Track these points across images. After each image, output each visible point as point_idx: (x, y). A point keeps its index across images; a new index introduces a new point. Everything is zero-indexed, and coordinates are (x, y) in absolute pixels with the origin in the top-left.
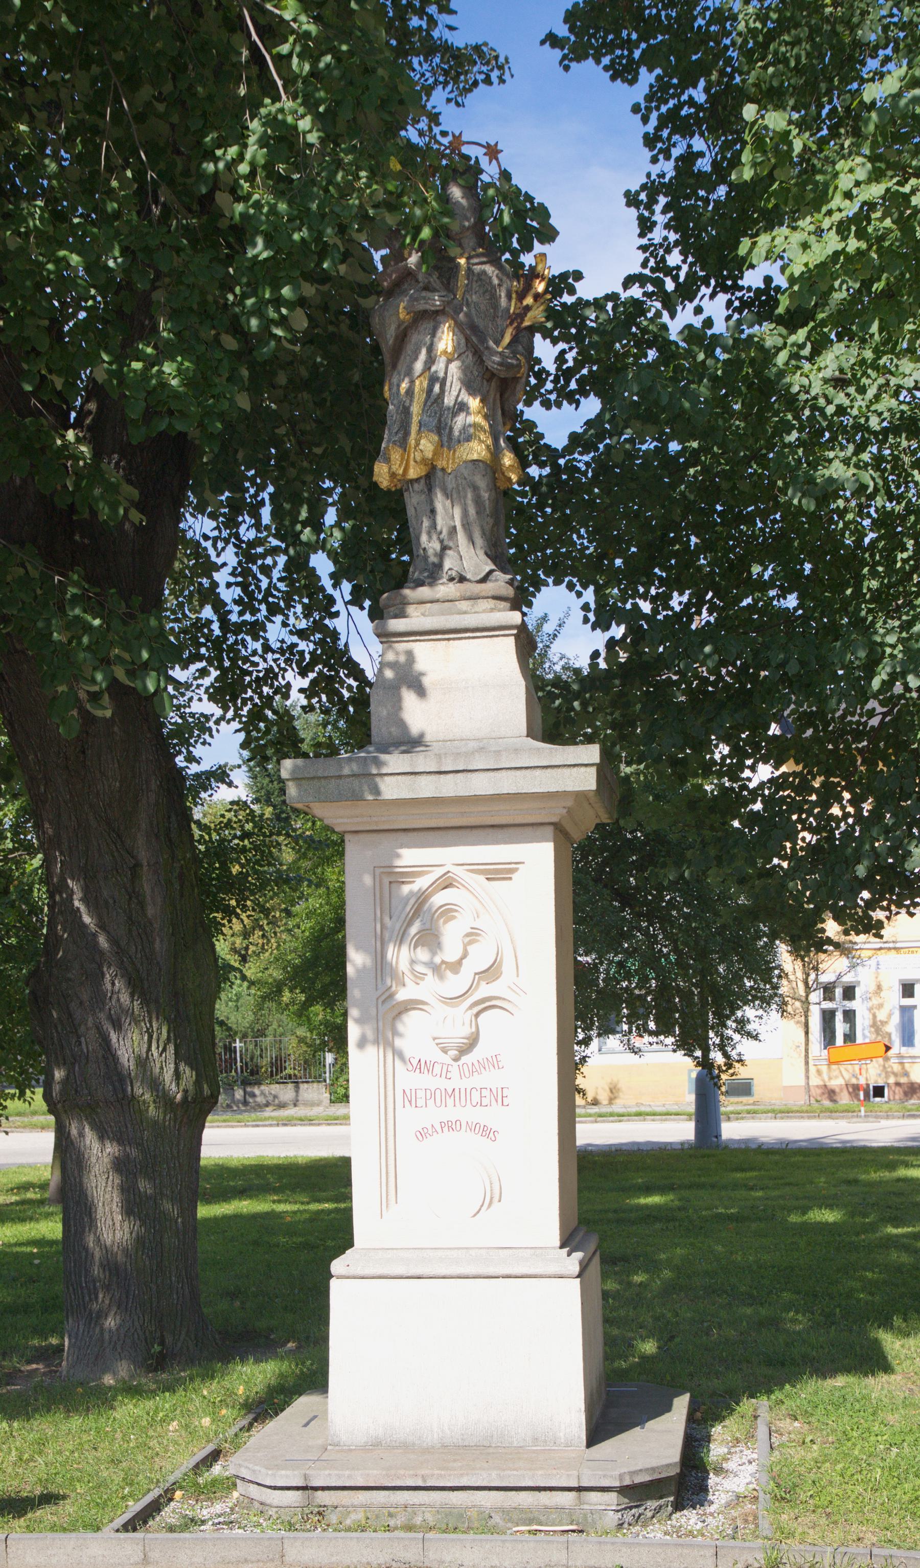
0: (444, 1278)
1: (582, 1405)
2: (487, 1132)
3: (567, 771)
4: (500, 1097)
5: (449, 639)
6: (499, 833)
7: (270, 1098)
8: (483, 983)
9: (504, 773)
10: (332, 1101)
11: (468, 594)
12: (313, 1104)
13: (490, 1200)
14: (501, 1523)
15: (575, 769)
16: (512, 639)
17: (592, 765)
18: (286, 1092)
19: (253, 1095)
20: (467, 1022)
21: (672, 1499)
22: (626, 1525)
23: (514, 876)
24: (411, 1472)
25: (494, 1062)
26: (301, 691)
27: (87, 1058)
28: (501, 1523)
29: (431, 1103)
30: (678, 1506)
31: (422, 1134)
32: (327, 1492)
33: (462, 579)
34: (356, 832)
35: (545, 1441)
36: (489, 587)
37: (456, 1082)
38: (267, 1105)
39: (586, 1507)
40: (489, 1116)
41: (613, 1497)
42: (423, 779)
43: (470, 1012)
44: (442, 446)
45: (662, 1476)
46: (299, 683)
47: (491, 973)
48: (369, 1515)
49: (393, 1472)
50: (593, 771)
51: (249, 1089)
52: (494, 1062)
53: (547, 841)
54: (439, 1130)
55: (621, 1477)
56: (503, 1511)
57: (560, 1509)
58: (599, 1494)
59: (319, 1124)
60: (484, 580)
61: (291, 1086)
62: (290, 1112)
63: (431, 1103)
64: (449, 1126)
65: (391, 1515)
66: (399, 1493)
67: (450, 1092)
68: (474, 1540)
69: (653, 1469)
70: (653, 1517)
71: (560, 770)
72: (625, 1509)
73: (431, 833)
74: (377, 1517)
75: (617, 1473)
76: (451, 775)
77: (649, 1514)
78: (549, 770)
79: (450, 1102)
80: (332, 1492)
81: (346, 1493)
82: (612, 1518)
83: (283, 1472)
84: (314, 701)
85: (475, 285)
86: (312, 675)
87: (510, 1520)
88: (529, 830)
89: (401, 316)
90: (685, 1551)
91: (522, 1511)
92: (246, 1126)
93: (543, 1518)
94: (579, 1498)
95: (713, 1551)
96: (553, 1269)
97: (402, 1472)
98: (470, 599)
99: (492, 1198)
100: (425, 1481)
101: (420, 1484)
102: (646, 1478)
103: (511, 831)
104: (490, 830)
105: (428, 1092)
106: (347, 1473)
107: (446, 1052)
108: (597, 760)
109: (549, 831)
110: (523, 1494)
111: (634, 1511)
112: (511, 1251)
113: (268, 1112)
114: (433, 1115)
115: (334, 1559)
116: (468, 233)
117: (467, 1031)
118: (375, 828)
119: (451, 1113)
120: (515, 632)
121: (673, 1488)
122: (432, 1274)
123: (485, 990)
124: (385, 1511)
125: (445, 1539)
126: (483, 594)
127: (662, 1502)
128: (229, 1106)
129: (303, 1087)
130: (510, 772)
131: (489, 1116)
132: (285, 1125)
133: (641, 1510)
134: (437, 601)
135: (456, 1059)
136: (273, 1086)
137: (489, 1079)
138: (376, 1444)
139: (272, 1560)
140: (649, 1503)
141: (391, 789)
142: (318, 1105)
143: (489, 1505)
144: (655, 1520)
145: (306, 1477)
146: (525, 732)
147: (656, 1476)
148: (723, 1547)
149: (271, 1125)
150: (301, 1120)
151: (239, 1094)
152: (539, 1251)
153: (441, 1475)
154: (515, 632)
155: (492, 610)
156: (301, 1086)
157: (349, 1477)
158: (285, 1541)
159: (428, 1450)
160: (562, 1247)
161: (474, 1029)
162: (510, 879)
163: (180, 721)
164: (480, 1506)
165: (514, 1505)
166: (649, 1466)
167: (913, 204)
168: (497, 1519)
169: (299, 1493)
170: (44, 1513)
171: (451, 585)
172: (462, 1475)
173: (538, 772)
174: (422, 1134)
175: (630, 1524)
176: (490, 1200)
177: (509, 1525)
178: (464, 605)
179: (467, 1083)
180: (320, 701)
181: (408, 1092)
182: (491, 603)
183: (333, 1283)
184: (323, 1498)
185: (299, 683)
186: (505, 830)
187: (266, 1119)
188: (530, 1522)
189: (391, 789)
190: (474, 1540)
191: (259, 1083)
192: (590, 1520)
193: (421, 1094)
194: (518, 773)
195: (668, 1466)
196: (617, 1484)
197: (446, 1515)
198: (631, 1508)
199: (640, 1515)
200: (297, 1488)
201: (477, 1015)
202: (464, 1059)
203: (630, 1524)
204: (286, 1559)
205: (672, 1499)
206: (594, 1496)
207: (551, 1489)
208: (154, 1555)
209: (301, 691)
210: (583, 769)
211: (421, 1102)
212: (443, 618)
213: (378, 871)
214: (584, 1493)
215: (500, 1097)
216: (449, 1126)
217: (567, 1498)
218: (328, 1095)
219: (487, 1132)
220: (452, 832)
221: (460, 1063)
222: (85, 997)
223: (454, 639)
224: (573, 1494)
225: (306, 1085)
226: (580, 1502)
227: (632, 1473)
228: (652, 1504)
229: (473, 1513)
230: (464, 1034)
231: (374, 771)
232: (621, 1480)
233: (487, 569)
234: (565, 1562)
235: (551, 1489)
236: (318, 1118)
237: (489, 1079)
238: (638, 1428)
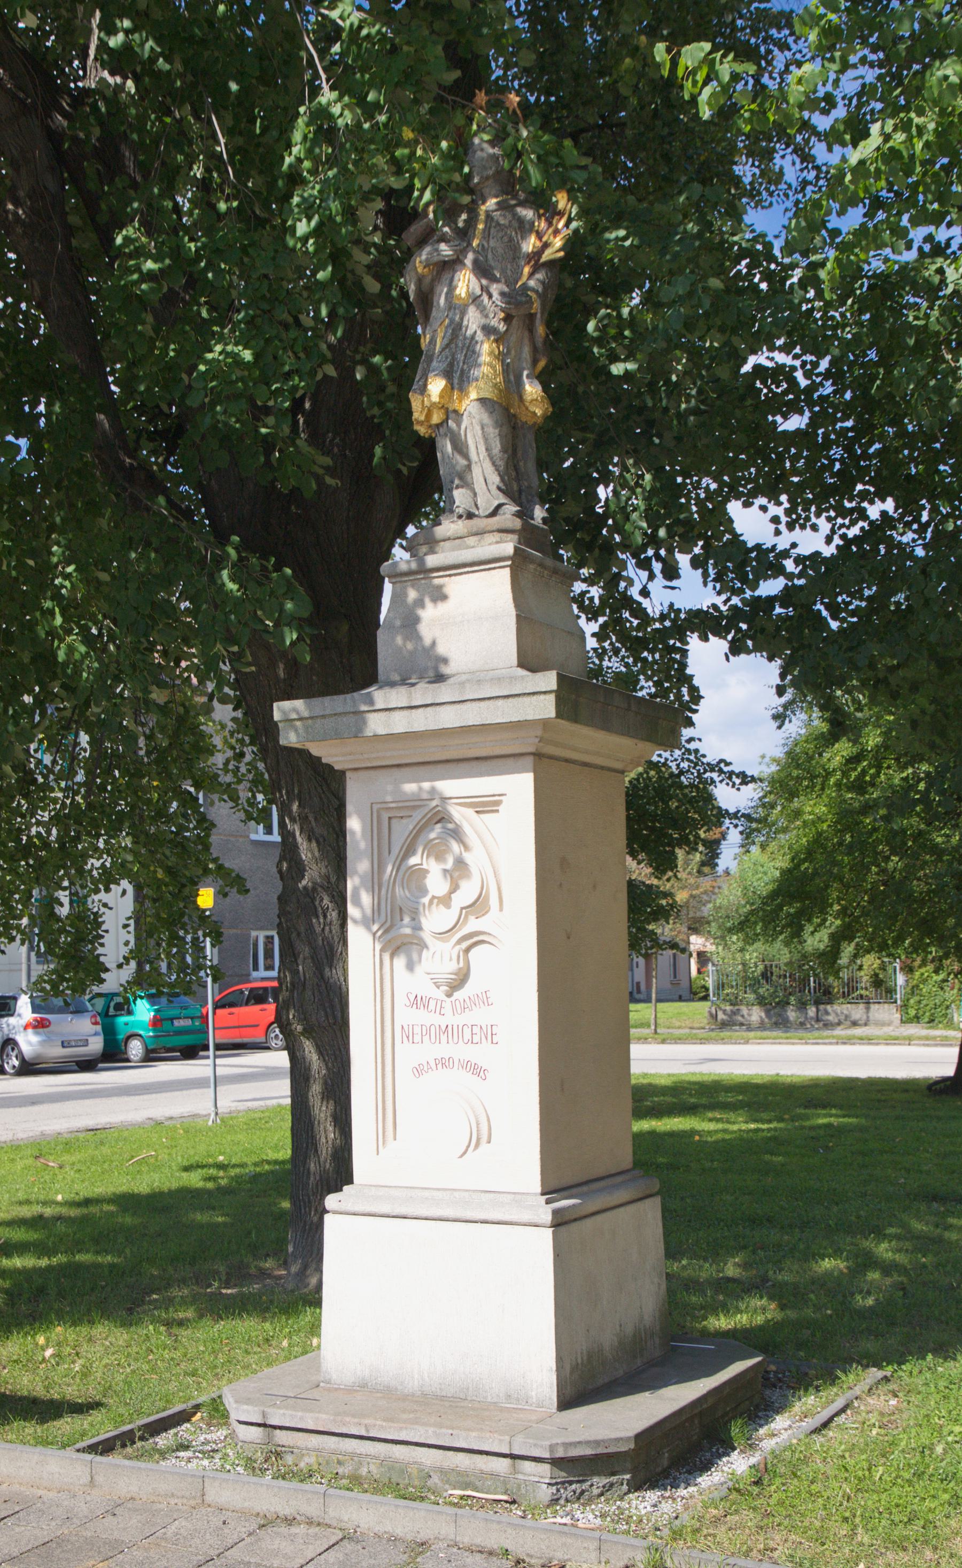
0: (426, 1219)
1: (553, 1364)
2: (478, 1071)
3: (526, 700)
4: (490, 1034)
5: (450, 576)
6: (483, 765)
7: (842, 1018)
8: (472, 919)
9: (468, 704)
10: (902, 1021)
11: (475, 529)
12: (883, 1024)
13: (476, 1142)
14: (440, 1484)
15: (535, 697)
16: (508, 570)
17: (550, 692)
18: (857, 1012)
19: (827, 1013)
20: (455, 957)
21: (628, 1476)
22: (562, 1502)
23: (500, 808)
24: (356, 1420)
25: (484, 999)
26: (594, 635)
27: (304, 984)
28: (440, 1484)
29: (426, 1038)
30: (637, 1486)
31: (419, 1071)
32: (284, 1432)
33: (470, 516)
34: (356, 769)
35: (518, 1400)
36: (495, 522)
37: (449, 1019)
38: (839, 1024)
39: (520, 1476)
40: (478, 1054)
41: (545, 1469)
42: (397, 715)
43: (458, 947)
44: (452, 388)
45: (609, 1450)
46: (590, 628)
47: (478, 906)
48: (320, 1460)
49: (339, 1418)
50: (552, 698)
51: (822, 1007)
52: (484, 999)
53: (527, 771)
54: (434, 1067)
55: (552, 1448)
56: (442, 1471)
57: (494, 1475)
58: (533, 1464)
59: (878, 1044)
60: (494, 513)
61: (862, 1006)
62: (858, 1031)
63: (426, 1038)
64: (443, 1063)
65: (339, 1463)
66: (347, 1440)
67: (443, 1028)
68: (370, 1501)
69: (597, 1443)
70: (602, 1494)
71: (520, 699)
72: (563, 1483)
73: (422, 768)
74: (328, 1463)
75: (548, 1443)
76: (421, 710)
77: (596, 1491)
78: (510, 700)
79: (444, 1038)
80: (289, 1432)
81: (301, 1434)
82: (545, 1493)
83: (245, 1407)
84: (606, 644)
85: (492, 230)
86: (601, 620)
87: (448, 1482)
88: (510, 761)
89: (420, 270)
90: (569, 1541)
91: (459, 1473)
92: (806, 1043)
93: (479, 1484)
94: (514, 1466)
95: (596, 1544)
96: (526, 1217)
97: (348, 1419)
98: (476, 534)
99: (478, 1140)
100: (368, 1431)
101: (364, 1433)
102: (588, 1451)
103: (494, 762)
104: (474, 763)
105: (476, 1030)
106: (300, 1414)
107: (438, 987)
108: (554, 686)
109: (529, 760)
110: (461, 1455)
111: (574, 1486)
112: (492, 1195)
113: (838, 1032)
114: (429, 1051)
115: (246, 1504)
116: (490, 182)
117: (453, 966)
118: (369, 765)
119: (444, 1050)
120: (509, 563)
121: (629, 1465)
122: (415, 1214)
123: (473, 925)
124: (334, 1458)
125: (343, 1497)
126: (489, 528)
127: (614, 1479)
128: (802, 1024)
129: (874, 1007)
130: (474, 704)
131: (478, 1054)
132: (844, 1043)
133: (585, 1486)
134: (449, 539)
135: (449, 995)
136: (845, 1006)
137: (479, 1016)
138: (364, 1385)
139: (194, 1498)
140: (595, 1479)
141: (376, 724)
142: (889, 1025)
143: (428, 1463)
144: (603, 1499)
145: (264, 1415)
146: (515, 662)
147: (600, 1450)
148: (606, 1541)
149: (831, 1044)
150: (861, 1039)
151: (812, 1011)
152: (518, 1197)
153: (382, 1427)
154: (509, 563)
155: (497, 542)
156: (872, 1006)
157: (301, 1418)
158: (206, 1480)
159: (405, 1398)
160: (543, 1194)
161: (461, 965)
162: (497, 811)
163: (624, 669)
164: (420, 1464)
165: (452, 1466)
166: (600, 1437)
167: (534, 57)
168: (435, 1480)
169: (261, 1429)
170: (66, 1425)
171: (460, 522)
172: (401, 1428)
173: (500, 702)
174: (419, 1071)
175: (567, 1501)
176: (476, 1142)
177: (447, 1486)
178: (471, 541)
179: (459, 1020)
180: (612, 644)
181: (406, 1028)
182: (497, 536)
183: (327, 1218)
184: (282, 1437)
185: (590, 628)
186: (489, 762)
187: (827, 1037)
188: (466, 1486)
189: (376, 724)
190: (370, 1501)
191: (830, 1002)
192: (523, 1491)
193: (417, 1030)
194: (482, 704)
195: (618, 1440)
196: (547, 1455)
197: (389, 1469)
198: (571, 1483)
199: (583, 1492)
200: (259, 1425)
201: (467, 950)
202: (457, 995)
203: (567, 1501)
204: (206, 1498)
205: (628, 1476)
206: (528, 1466)
207: (487, 1453)
208: (99, 1479)
209: (594, 635)
210: (542, 697)
211: (417, 1038)
212: (456, 553)
213: (375, 807)
214: (518, 1462)
215: (490, 1034)
216: (443, 1063)
217: (502, 1465)
218: (898, 1016)
219: (478, 1071)
220: (440, 766)
221: (453, 999)
222: (302, 929)
223: (455, 575)
224: (507, 1461)
225: (877, 1006)
226: (515, 1470)
227: (566, 1445)
228: (599, 1481)
229: (413, 1470)
230: (450, 970)
231: (364, 708)
232: (551, 1451)
233: (496, 503)
234: (452, 1537)
235: (487, 1453)
236: (878, 1038)
237: (479, 1016)
238: (647, 1394)
